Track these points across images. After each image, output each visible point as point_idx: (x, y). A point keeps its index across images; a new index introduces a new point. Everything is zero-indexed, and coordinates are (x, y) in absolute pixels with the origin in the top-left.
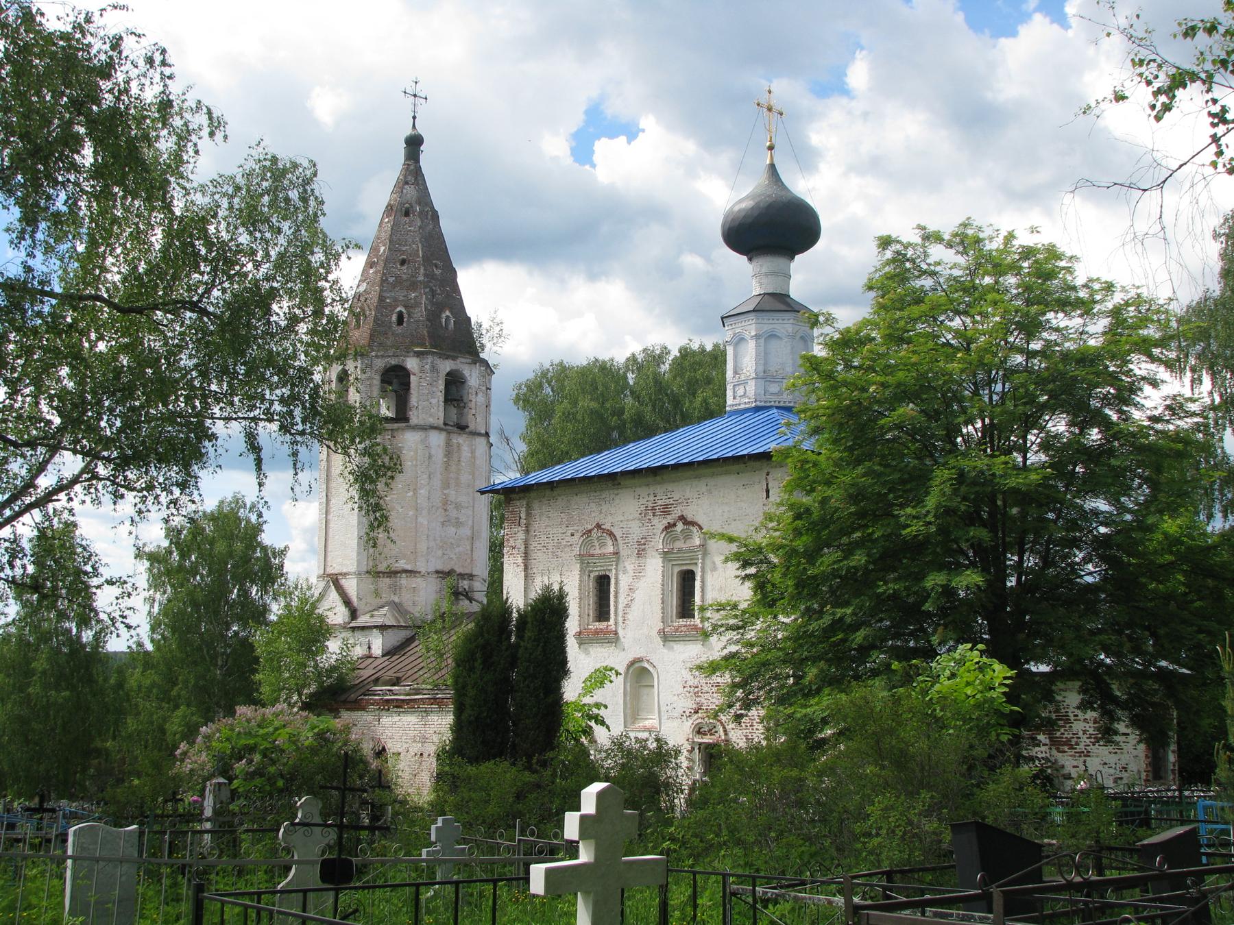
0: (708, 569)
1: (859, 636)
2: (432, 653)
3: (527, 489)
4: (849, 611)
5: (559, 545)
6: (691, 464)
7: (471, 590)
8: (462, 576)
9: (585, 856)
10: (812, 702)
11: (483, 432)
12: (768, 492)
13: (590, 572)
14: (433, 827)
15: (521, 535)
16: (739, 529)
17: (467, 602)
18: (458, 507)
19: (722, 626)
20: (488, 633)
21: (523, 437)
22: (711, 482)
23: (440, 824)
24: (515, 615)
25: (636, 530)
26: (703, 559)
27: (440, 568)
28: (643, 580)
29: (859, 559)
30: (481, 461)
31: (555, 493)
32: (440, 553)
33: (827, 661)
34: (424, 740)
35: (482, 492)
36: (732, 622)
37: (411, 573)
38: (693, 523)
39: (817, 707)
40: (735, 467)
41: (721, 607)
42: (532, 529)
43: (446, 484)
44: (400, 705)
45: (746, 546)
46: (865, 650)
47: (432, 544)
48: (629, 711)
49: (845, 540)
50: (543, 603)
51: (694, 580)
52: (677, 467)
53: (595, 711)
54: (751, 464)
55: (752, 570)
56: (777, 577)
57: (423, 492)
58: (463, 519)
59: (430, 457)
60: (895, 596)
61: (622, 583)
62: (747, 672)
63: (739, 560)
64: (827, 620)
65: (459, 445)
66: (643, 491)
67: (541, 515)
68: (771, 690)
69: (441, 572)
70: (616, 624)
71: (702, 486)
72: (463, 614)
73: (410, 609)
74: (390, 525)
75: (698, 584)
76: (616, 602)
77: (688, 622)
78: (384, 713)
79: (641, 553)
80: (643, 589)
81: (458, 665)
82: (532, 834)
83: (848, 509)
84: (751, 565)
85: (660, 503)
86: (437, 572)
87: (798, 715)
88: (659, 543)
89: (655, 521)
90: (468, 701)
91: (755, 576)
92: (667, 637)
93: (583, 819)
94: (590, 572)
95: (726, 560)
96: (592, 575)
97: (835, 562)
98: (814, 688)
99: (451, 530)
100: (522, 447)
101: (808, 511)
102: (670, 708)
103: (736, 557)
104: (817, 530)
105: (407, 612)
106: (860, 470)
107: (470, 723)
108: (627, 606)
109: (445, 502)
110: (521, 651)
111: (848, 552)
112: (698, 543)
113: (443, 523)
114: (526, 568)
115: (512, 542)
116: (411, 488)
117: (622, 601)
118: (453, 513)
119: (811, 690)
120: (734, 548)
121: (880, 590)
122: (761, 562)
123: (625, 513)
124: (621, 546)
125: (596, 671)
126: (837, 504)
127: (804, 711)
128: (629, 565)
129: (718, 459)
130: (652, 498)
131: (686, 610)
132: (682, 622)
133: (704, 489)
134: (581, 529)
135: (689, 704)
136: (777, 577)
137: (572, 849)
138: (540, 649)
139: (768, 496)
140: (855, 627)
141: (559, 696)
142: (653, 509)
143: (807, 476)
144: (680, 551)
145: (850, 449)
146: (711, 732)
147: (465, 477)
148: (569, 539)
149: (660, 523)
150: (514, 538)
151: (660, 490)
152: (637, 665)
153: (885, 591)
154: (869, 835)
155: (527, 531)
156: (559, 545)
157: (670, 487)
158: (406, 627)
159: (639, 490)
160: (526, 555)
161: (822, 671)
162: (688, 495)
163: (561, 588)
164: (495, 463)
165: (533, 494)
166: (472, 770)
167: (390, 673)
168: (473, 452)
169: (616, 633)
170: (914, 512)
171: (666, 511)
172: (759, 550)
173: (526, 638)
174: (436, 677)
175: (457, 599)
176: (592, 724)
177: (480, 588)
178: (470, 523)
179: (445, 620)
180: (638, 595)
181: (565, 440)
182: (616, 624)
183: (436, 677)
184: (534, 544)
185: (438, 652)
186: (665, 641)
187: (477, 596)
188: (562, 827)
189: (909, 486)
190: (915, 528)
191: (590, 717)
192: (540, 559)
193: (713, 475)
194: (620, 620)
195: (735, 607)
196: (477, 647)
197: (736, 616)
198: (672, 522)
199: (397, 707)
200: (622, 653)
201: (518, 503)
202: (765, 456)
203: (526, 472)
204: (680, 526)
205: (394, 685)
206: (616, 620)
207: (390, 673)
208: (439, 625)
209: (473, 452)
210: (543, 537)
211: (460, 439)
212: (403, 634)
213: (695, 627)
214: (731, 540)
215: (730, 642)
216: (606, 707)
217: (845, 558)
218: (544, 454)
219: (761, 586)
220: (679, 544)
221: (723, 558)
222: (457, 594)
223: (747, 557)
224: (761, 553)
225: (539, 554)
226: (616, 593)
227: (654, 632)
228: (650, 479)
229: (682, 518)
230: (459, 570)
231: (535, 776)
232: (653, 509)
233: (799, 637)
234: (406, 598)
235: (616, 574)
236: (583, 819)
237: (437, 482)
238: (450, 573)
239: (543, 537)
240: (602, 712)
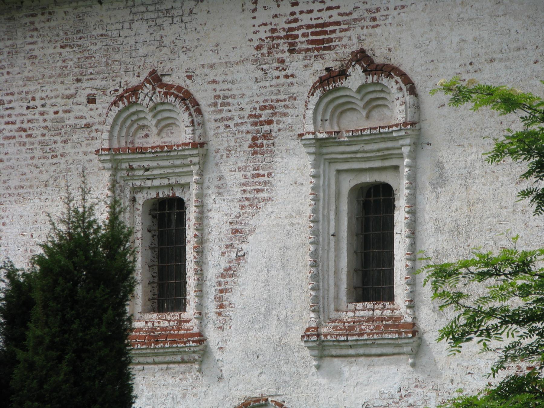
0: (426, 177)
5: (57, 128)
19: (492, 313)
25: (248, 87)
26: (414, 155)
28: (268, 208)
36: (516, 303)
38: (388, 70)
41: (489, 268)
51: (390, 207)
61: (213, 216)
63: (529, 153)
70: (201, 315)
75: (400, 217)
76: (200, 263)
79: (260, 144)
85: (305, 19)
88: (303, 116)
89: (295, 64)
92: (324, 346)
95: (499, 153)
96: (141, 198)
103: (524, 144)
108: (229, 272)
117: (216, 261)
120: (516, 122)
124: (211, 126)
128: (231, 170)
131: (372, 278)
132: (363, 310)
134: (112, 85)
138: (64, 367)
142: (290, 35)
144: (357, 136)
148: (84, 110)
149: (306, 72)
169: (201, 339)
171: (321, 43)
173: (30, 343)
180: (256, 246)
182: (201, 315)
186: (320, 357)
194: (211, 307)
195: (523, 266)
198: (335, 66)
200: (217, 389)
204: (356, 78)
206: (200, 307)
213: (395, 323)
214: (510, 103)
215: (512, 353)
220: (354, 122)
221: (491, 147)
227: (295, 335)
229: (361, 57)
232: (290, 35)
235: (201, 196)
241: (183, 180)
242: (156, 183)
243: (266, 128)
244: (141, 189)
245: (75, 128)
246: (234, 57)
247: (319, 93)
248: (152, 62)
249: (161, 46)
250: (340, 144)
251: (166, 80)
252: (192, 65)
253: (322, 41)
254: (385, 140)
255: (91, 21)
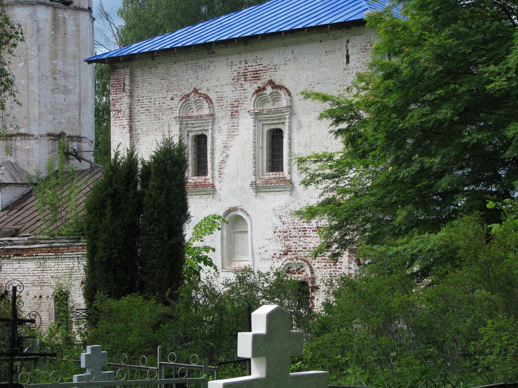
0: (294, 127)
1: (444, 183)
2: (48, 206)
3: (131, 58)
4: (437, 161)
5: (160, 109)
6: (278, 34)
7: (80, 150)
8: (71, 138)
9: (257, 372)
10: (400, 241)
11: (86, 7)
12: (348, 57)
13: (189, 132)
14: (83, 356)
15: (126, 100)
16: (334, 90)
17: (76, 161)
18: (66, 76)
19: (319, 175)
20: (117, 183)
21: (121, 13)
22: (297, 49)
23: (89, 352)
24: (140, 166)
25: (230, 94)
26: (290, 118)
27: (51, 131)
28: (237, 138)
29: (445, 112)
30: (85, 33)
31: (156, 62)
32: (51, 117)
33: (415, 204)
34: (42, 284)
35: (89, 62)
36: (328, 171)
37: (25, 136)
38: (281, 87)
39: (405, 246)
40: (319, 36)
41: (318, 159)
42: (136, 94)
43: (54, 56)
44: (19, 253)
45: (338, 103)
46: (449, 195)
47: (43, 109)
48: (225, 254)
49: (428, 97)
50: (165, 155)
51: (282, 137)
52: (266, 36)
53: (204, 253)
54: (332, 33)
55: (344, 125)
56: (369, 130)
57: (33, 62)
58: (70, 87)
59: (39, 30)
60: (478, 146)
61: (217, 141)
62: (343, 217)
63: (332, 117)
64: (415, 167)
65: (64, 20)
66: (236, 59)
67: (144, 81)
68: (365, 231)
69: (53, 135)
70: (213, 177)
71: (288, 53)
72: (74, 172)
73: (26, 168)
74: (14, 88)
75: (285, 141)
76: (212, 158)
77: (277, 175)
78: (5, 261)
80: (235, 149)
81: (90, 212)
82: (172, 359)
83: (436, 68)
84: (343, 120)
85: (250, 69)
86: (49, 135)
87: (390, 253)
89: (247, 85)
90: (100, 244)
91: (346, 130)
92: (258, 188)
93: (256, 337)
94: (189, 132)
96: (191, 135)
97: (423, 115)
98: (403, 228)
99: (61, 97)
100: (120, 23)
101: (397, 71)
102: (262, 250)
103: (330, 114)
104: (401, 87)
105: (23, 171)
106: (447, 31)
107: (102, 263)
108: (223, 162)
109: (54, 72)
110: (145, 199)
111: (435, 105)
112: (285, 105)
113: (53, 91)
114: (131, 129)
115: (117, 107)
116: (22, 58)
118: (62, 82)
119: (400, 230)
120: (327, 106)
121: (466, 140)
122: (352, 117)
123: (220, 79)
124: (216, 108)
125: (205, 219)
126: (426, 64)
127: (395, 249)
128: (223, 124)
129: (303, 29)
130: (243, 65)
131: (275, 163)
132: (272, 175)
133: (290, 56)
134: (180, 94)
135: (279, 247)
136: (369, 130)
137: (244, 365)
138: (163, 196)
139: (348, 62)
140: (439, 175)
141: (182, 237)
142: (245, 75)
143: (398, 39)
144: (270, 111)
145: (436, 14)
146: (299, 271)
147: (71, 49)
148: (169, 102)
149: (251, 88)
150: (120, 102)
151: (250, 58)
152: (232, 214)
153: (470, 140)
154: (481, 353)
155: (131, 96)
156: (160, 109)
157: (260, 54)
158: (22, 185)
159: (231, 58)
160: (131, 118)
161: (410, 213)
162: (276, 61)
163: (180, 141)
164: (98, 37)
165: (136, 63)
166: (112, 304)
167: (10, 225)
168: (77, 26)
169: (213, 186)
170: (497, 69)
171: (256, 77)
172: (350, 107)
174: (52, 228)
175: (68, 159)
176: (202, 264)
177: (87, 148)
178: (77, 90)
179: (59, 178)
180: (231, 152)
181: (160, 15)
182: (213, 177)
183: (52, 228)
184: (137, 108)
185: (53, 205)
186: (257, 192)
187: (85, 156)
188: (235, 347)
189: (490, 46)
190: (499, 84)
191: (199, 259)
192: (143, 121)
193: (298, 43)
194: (217, 174)
195: (330, 158)
196: (107, 196)
197: (331, 167)
198: (261, 86)
199: (17, 255)
201: (122, 71)
202: (360, 23)
203: (125, 43)
204: (269, 90)
205: (14, 236)
206: (213, 174)
207: (10, 225)
208: (53, 181)
209: (77, 26)
210: (146, 102)
211: (65, 14)
212: (20, 191)
213: (284, 180)
214: (325, 98)
215: (327, 190)
216: (214, 250)
217: (432, 113)
218: (140, 26)
219: (352, 139)
220: (268, 106)
221: (318, 114)
222: (67, 154)
223: (339, 113)
224: (351, 110)
225: (143, 117)
226: (213, 150)
228: (242, 48)
229: (271, 83)
230: (68, 133)
231: (167, 308)
232: (245, 75)
233: (389, 184)
234: (21, 159)
235: (213, 134)
236: (256, 337)
237: (46, 53)
238: (61, 136)
239: (146, 102)
240: (210, 255)
241: (206, 128)
242: (196, 129)
243: (236, 109)
244: (191, 131)
245: (166, 109)
246: (224, 83)
247: (255, 96)
248: (194, 85)
249: (198, 79)
250: (263, 114)
251: (199, 91)
252: (209, 86)
253: (257, 77)
254: (279, 113)
255: (172, 70)
